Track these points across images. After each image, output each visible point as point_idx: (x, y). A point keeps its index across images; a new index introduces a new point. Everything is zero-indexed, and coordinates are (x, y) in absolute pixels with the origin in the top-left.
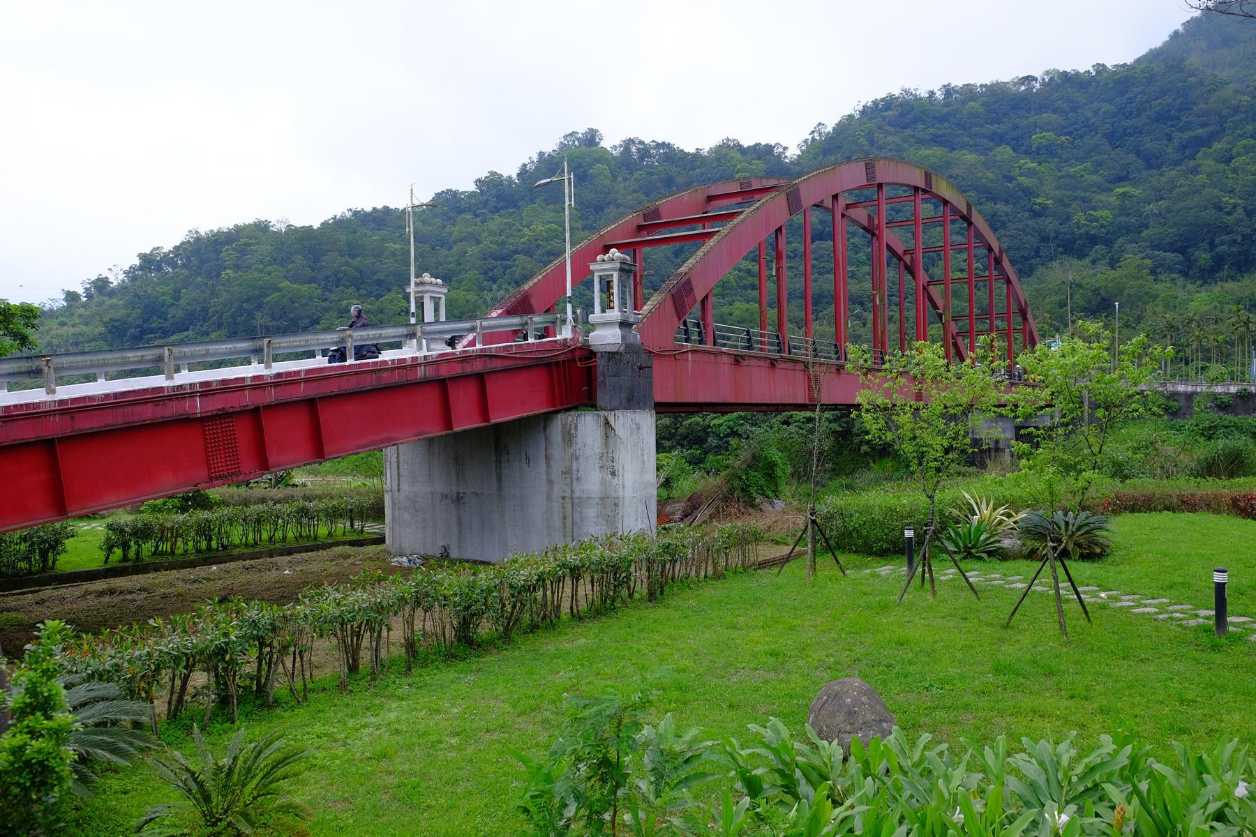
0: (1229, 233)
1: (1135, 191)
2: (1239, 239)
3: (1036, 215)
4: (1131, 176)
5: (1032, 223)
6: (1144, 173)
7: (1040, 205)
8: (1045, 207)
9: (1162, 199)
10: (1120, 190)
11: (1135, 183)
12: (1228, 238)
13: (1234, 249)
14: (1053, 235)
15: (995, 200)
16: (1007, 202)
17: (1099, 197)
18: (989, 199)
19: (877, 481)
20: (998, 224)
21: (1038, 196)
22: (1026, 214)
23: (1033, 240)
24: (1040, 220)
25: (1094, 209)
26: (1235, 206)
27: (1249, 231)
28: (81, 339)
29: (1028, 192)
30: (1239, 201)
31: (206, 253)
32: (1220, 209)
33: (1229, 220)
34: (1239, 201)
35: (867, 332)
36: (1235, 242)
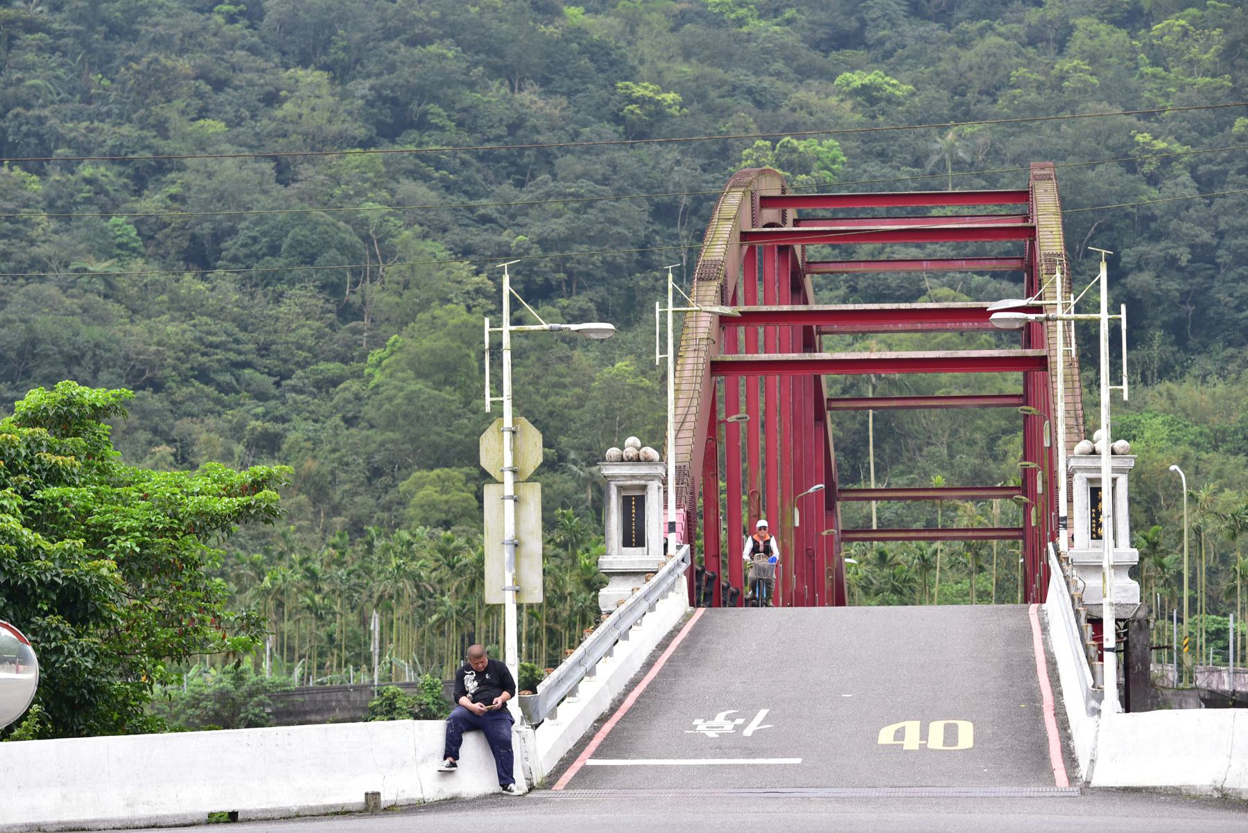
0: (1156, 237)
1: (896, 86)
2: (1185, 257)
3: (636, 133)
4: (871, 35)
5: (626, 158)
6: (906, 27)
7: (642, 101)
8: (658, 113)
9: (968, 117)
10: (857, 79)
11: (886, 57)
12: (1155, 250)
13: (1173, 285)
14: (685, 200)
15: (512, 76)
16: (545, 84)
17: (801, 94)
18: (496, 71)
19: (52, 825)
20: (529, 156)
21: (631, 75)
22: (608, 129)
23: (633, 214)
24: (646, 151)
25: (793, 129)
26: (1167, 160)
27: (1206, 236)
28: (1072, 413)
29: (610, 62)
30: (1178, 148)
31: (1120, 698)
32: (1131, 166)
33: (1152, 197)
34: (1178, 148)
35: (721, 558)
36: (1172, 262)
